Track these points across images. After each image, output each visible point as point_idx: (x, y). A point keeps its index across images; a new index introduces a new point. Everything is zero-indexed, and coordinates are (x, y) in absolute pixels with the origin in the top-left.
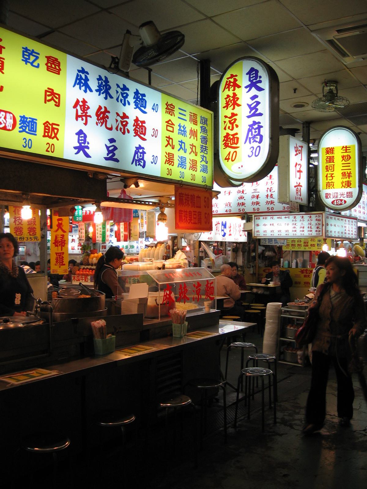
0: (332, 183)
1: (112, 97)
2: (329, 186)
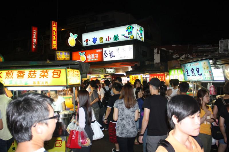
0: (12, 73)
1: (196, 139)
2: (8, 75)
